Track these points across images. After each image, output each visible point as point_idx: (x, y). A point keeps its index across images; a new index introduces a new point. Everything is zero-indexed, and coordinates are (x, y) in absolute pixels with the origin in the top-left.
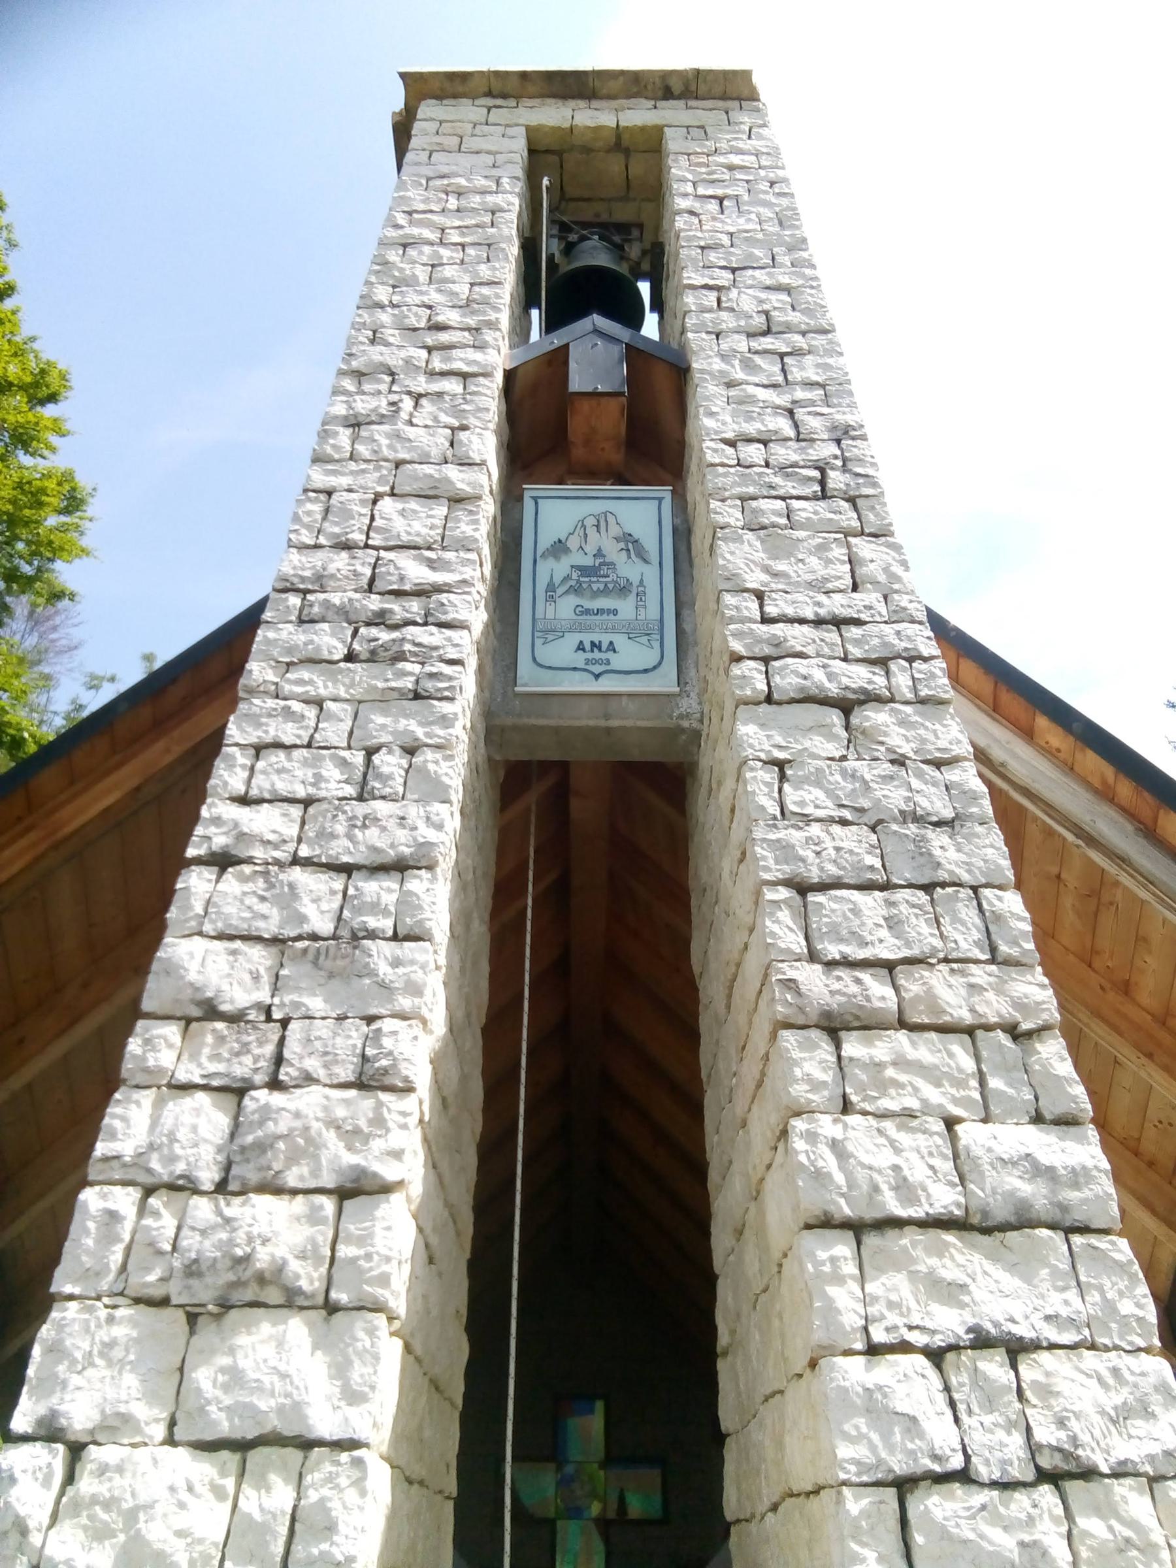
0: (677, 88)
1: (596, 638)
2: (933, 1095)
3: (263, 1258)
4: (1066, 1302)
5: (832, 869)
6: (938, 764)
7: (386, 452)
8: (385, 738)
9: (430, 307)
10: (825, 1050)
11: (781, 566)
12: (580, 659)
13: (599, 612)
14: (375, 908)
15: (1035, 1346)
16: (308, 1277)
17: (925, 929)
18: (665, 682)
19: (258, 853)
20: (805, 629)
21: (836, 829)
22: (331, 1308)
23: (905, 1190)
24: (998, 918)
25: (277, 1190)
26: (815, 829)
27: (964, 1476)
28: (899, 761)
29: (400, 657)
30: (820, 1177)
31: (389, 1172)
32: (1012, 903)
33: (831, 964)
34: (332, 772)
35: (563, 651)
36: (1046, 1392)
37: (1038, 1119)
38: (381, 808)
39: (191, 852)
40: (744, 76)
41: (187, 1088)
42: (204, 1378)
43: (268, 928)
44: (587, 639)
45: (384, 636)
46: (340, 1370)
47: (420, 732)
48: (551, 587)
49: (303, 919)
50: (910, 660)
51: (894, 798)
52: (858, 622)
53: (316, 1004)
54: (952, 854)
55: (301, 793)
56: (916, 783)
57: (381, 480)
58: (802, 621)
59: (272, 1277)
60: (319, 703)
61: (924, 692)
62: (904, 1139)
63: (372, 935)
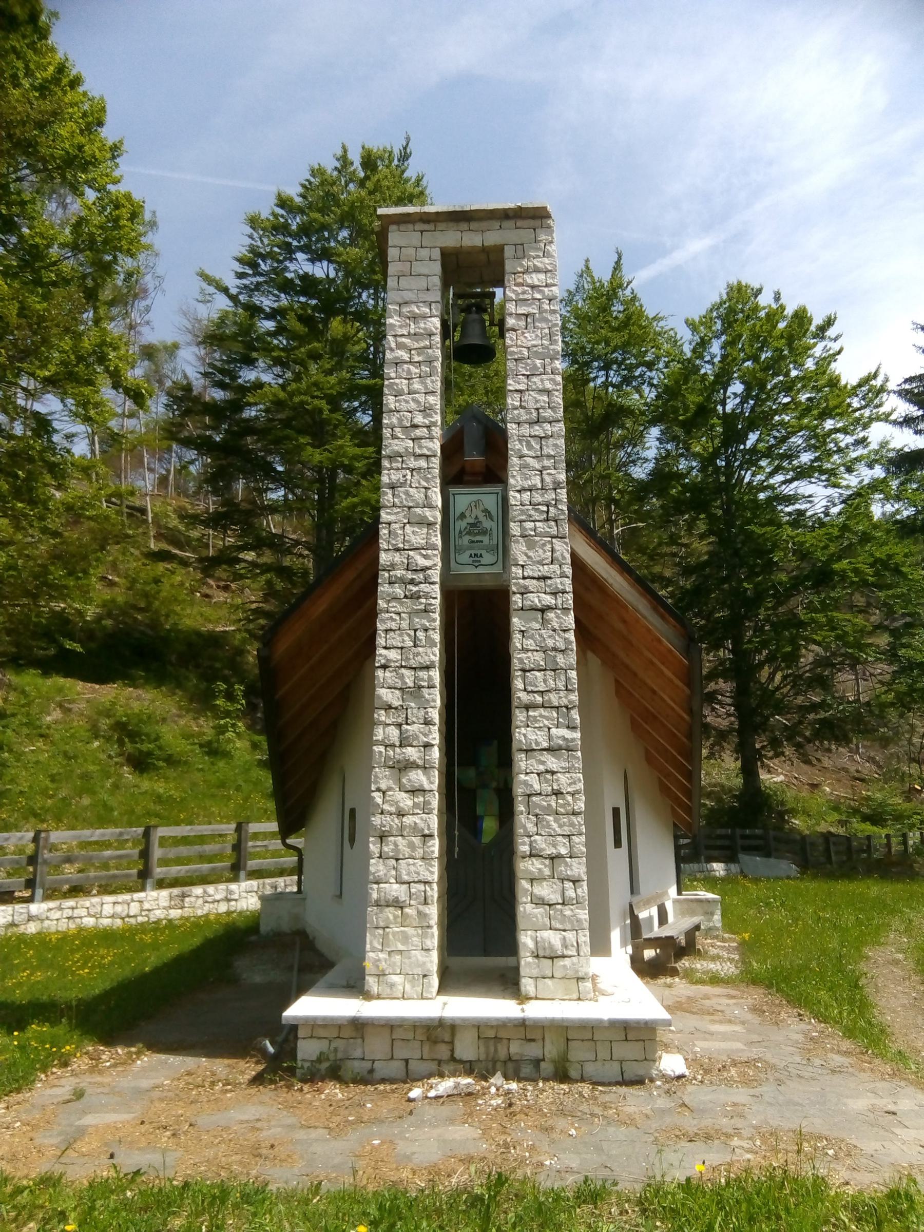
0: (511, 214)
1: (476, 552)
2: (546, 722)
3: (412, 759)
4: (563, 764)
5: (532, 666)
6: (564, 631)
7: (405, 502)
8: (419, 627)
9: (410, 412)
10: (525, 714)
11: (531, 554)
12: (470, 561)
13: (477, 541)
14: (423, 680)
15: (557, 772)
16: (420, 762)
17: (552, 682)
18: (497, 569)
19: (392, 664)
20: (534, 581)
21: (535, 653)
22: (426, 768)
23: (537, 743)
24: (569, 678)
25: (412, 746)
26: (530, 654)
27: (540, 794)
28: (554, 630)
29: (419, 597)
30: (521, 741)
31: (433, 742)
32: (573, 674)
33: (529, 692)
34: (406, 638)
35: (465, 557)
36: (557, 780)
37: (568, 727)
38: (420, 649)
39: (377, 665)
40: (544, 209)
41: (389, 725)
42: (404, 781)
43: (399, 685)
44: (473, 552)
45: (415, 589)
46: (429, 779)
47: (427, 624)
48: (460, 532)
49: (406, 683)
50: (563, 593)
51: (550, 643)
52: (550, 578)
53: (413, 705)
54: (562, 660)
55: (400, 646)
56: (557, 638)
57: (405, 517)
58: (534, 578)
59: (414, 763)
60: (399, 614)
61: (565, 606)
62: (539, 733)
63: (423, 687)
